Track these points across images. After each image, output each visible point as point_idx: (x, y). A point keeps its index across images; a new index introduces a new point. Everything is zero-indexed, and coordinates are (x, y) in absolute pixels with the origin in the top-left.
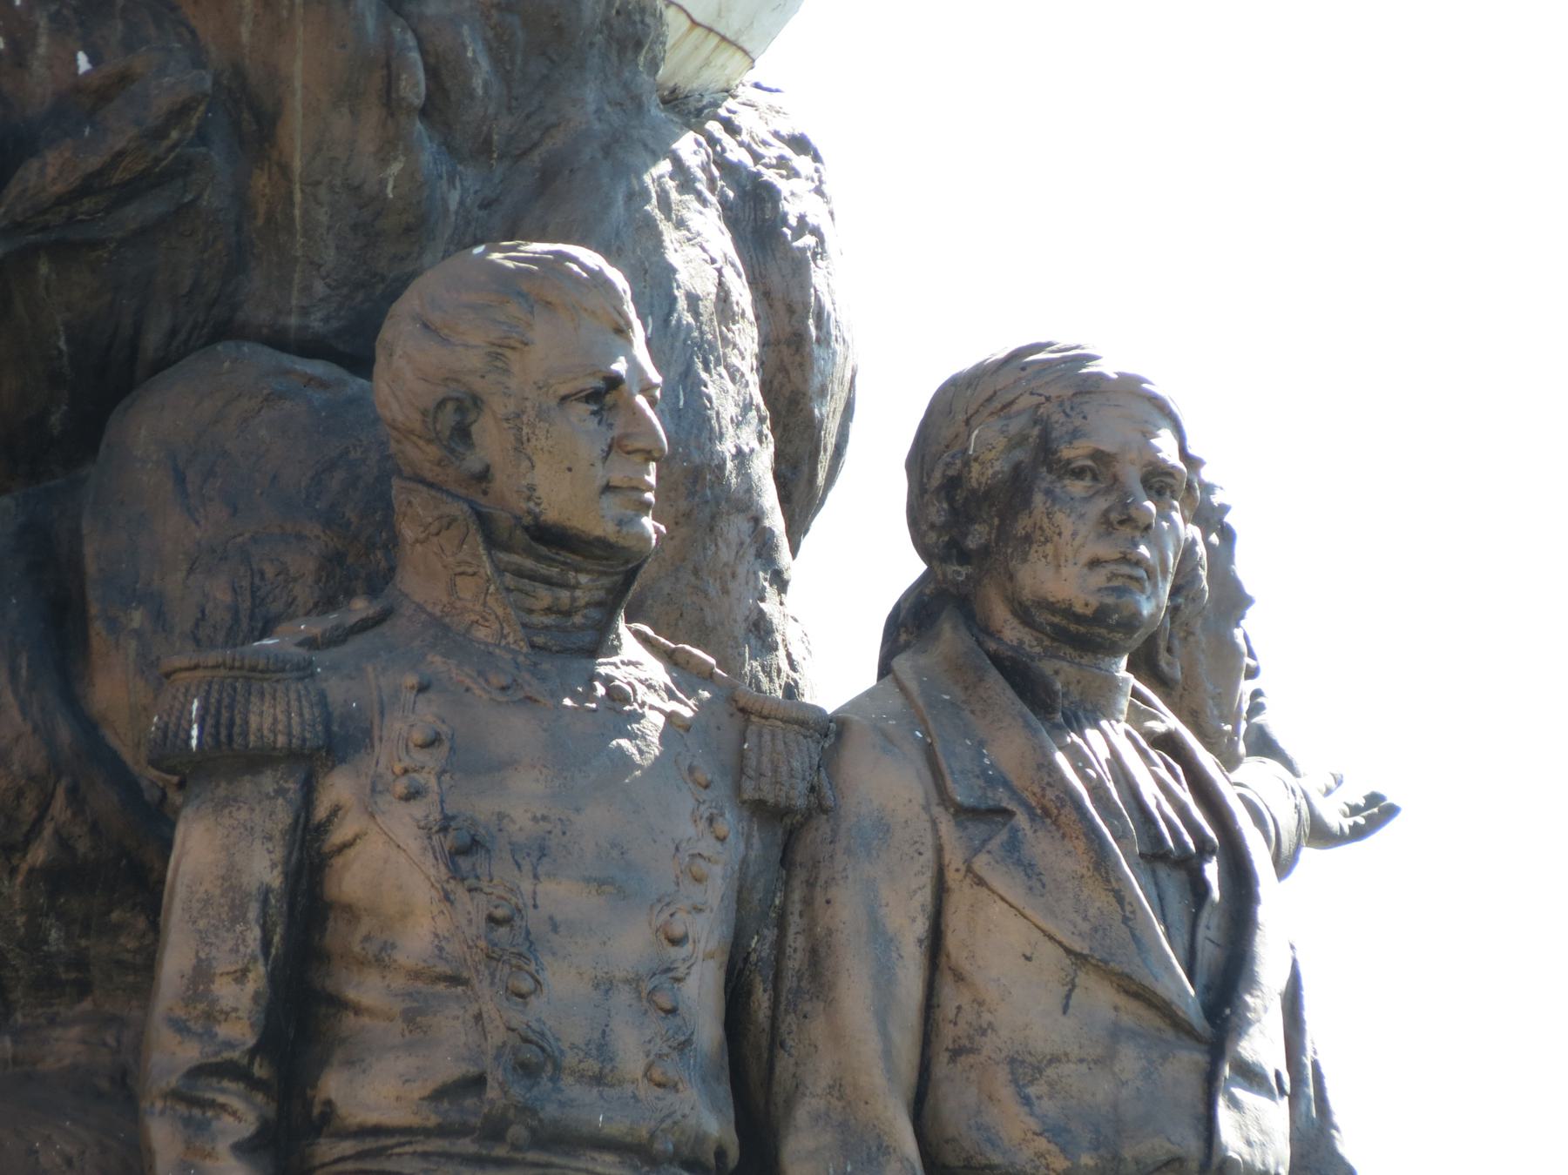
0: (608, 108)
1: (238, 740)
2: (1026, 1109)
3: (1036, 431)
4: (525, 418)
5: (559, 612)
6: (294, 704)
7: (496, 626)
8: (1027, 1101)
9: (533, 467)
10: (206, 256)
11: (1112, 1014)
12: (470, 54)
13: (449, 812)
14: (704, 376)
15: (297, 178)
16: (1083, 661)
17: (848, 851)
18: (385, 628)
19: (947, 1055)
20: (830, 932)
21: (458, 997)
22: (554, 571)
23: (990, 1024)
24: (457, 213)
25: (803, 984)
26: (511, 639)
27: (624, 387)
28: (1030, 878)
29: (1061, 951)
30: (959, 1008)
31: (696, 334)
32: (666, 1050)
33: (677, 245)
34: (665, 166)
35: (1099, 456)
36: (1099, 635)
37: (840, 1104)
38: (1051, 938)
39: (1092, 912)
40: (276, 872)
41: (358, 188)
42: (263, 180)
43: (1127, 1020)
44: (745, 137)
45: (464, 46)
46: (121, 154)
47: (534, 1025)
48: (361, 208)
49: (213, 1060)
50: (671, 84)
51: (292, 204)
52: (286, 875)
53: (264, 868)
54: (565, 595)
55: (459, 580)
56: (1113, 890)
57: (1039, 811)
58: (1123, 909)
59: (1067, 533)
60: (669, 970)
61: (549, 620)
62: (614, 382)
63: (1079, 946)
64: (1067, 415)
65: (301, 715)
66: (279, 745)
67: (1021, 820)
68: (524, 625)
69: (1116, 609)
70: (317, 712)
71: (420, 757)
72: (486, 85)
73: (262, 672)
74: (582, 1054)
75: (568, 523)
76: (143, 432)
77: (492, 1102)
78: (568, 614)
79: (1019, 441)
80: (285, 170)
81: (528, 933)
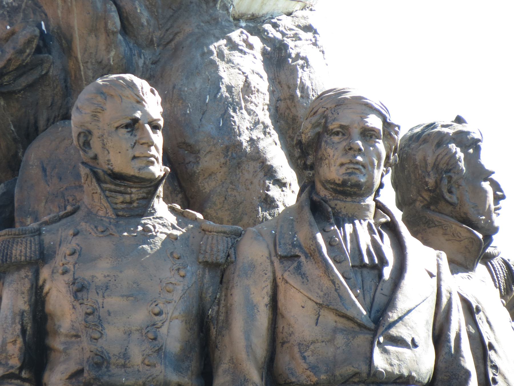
0: (202, 24)
1: (8, 260)
2: (304, 361)
3: (323, 121)
4: (104, 136)
5: (127, 203)
6: (28, 245)
7: (105, 210)
8: (304, 358)
9: (109, 153)
10: (55, 92)
11: (335, 324)
12: (139, 11)
13: (76, 277)
14: (233, 114)
15: (80, 61)
16: (347, 200)
17: (239, 276)
18: (75, 215)
19: (280, 344)
20: (231, 305)
21: (78, 342)
22: (122, 189)
23: (292, 332)
24: (143, 67)
25: (224, 324)
26: (109, 214)
27: (141, 122)
28: (303, 278)
29: (314, 304)
30: (283, 327)
31: (230, 100)
32: (150, 353)
33: (225, 69)
34: (223, 42)
35: (341, 126)
36: (348, 190)
37: (233, 365)
38: (310, 299)
39: (324, 288)
40: (26, 305)
41: (101, 62)
42: (72, 63)
43: (340, 326)
44: (281, 28)
45: (136, 8)
46: (10, 60)
47: (99, 349)
48: (103, 69)
49: (6, 373)
50: (251, 13)
51: (80, 70)
52: (30, 305)
53: (23, 304)
54: (128, 197)
55: (94, 195)
56: (331, 280)
57: (309, 255)
58: (335, 286)
59: (331, 155)
60: (154, 325)
61: (124, 206)
62: (136, 120)
63: (319, 301)
64: (333, 114)
65: (31, 249)
66: (22, 260)
67: (303, 259)
68: (114, 209)
69: (349, 180)
70: (37, 247)
71: (69, 258)
72: (148, 21)
73: (18, 235)
74: (117, 358)
75: (122, 172)
76: (33, 156)
77: (85, 378)
78: (131, 203)
79: (318, 125)
80: (76, 58)
81: (99, 317)
